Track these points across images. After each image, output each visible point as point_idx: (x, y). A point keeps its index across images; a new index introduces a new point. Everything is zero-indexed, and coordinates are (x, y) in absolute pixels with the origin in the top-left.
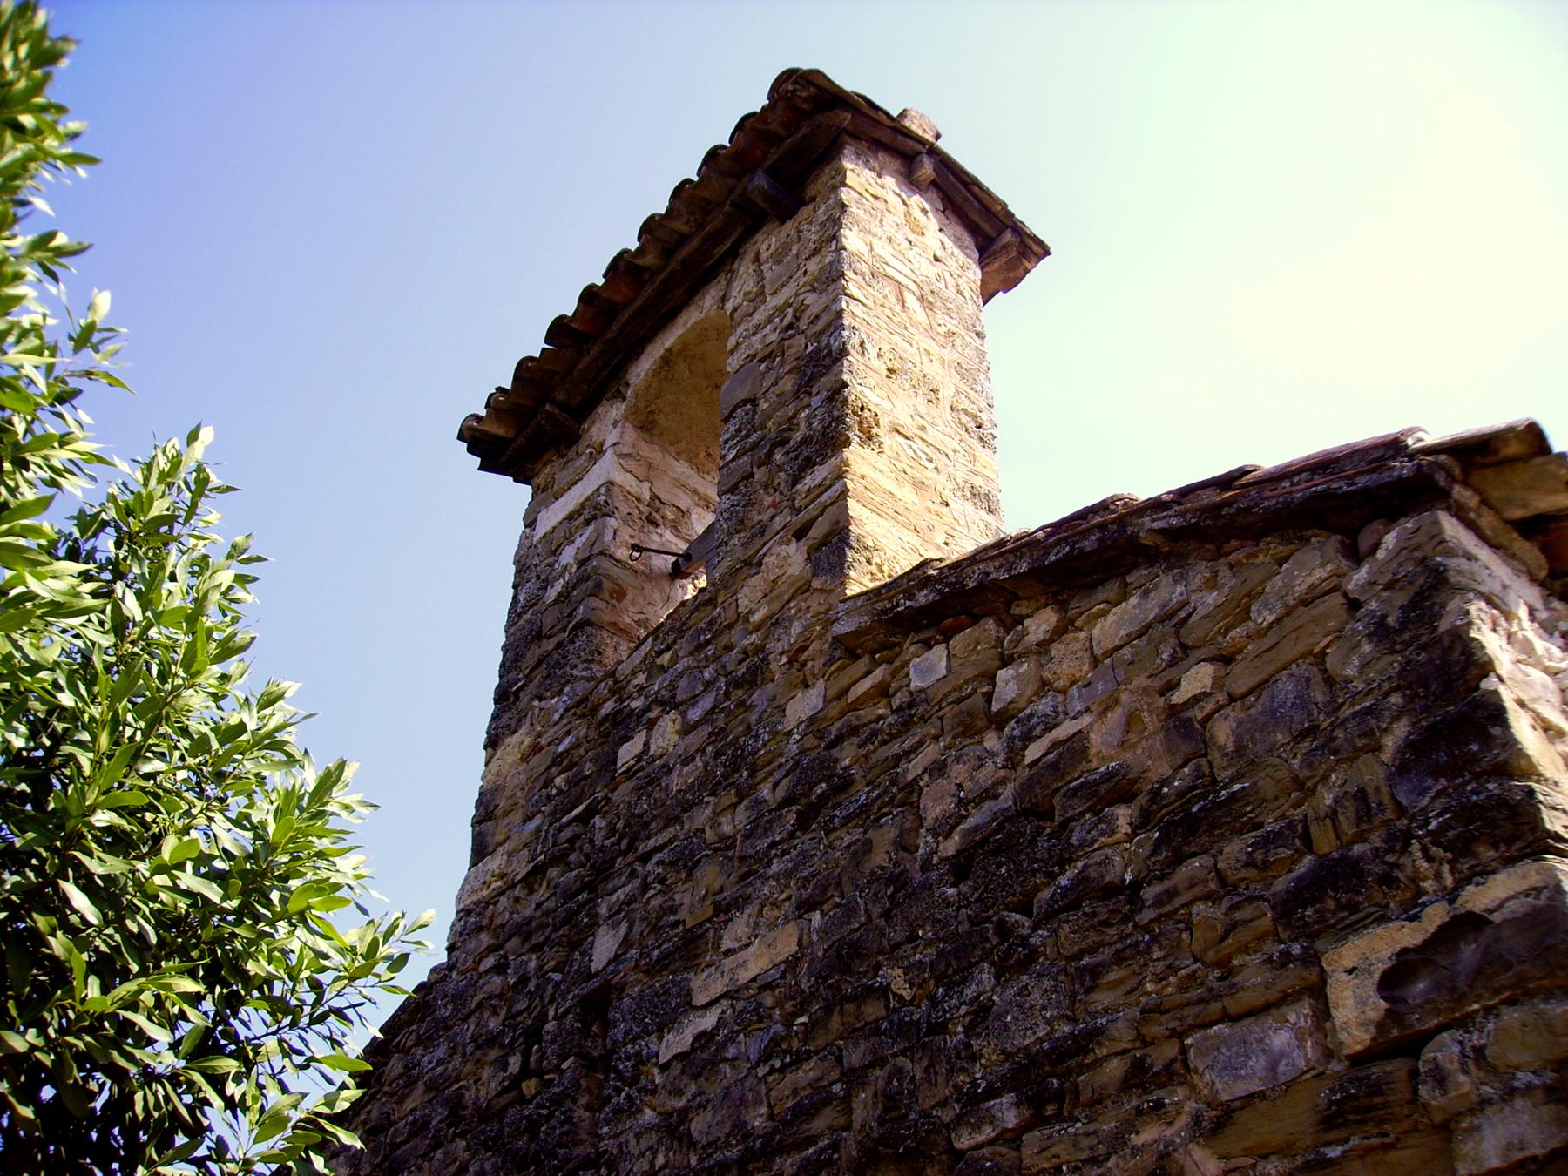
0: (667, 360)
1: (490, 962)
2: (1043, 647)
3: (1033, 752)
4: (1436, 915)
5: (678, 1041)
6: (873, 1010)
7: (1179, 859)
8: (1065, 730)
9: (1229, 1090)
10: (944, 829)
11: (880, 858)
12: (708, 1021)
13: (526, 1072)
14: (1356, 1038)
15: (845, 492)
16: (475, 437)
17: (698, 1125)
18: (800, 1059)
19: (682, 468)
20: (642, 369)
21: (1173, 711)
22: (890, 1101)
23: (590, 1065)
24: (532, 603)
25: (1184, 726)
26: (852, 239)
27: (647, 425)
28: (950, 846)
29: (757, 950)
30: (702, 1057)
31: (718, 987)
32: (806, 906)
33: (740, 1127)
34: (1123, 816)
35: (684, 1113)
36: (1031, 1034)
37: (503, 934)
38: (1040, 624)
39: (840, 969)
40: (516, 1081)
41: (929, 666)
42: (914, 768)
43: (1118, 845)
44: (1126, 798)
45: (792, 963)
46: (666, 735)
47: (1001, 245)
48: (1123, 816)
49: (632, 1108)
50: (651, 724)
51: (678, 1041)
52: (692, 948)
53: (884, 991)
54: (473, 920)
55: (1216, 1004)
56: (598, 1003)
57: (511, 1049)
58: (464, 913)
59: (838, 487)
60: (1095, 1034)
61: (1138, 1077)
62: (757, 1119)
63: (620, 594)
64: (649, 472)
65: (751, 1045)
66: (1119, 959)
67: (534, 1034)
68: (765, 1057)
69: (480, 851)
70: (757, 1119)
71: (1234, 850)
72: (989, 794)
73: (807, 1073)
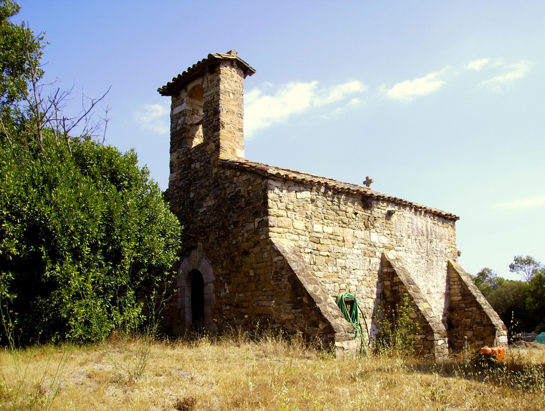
0: (194, 87)
1: (175, 191)
2: (239, 176)
3: (237, 189)
4: (262, 219)
5: (202, 210)
6: (222, 213)
7: (247, 206)
8: (239, 188)
9: (248, 229)
10: (229, 194)
11: (223, 195)
12: (205, 209)
13: (183, 209)
14: (256, 227)
15: (219, 139)
16: (159, 90)
17: (204, 221)
18: (215, 216)
19: (197, 102)
20: (190, 87)
21: (248, 191)
22: (223, 223)
23: (191, 209)
24: (175, 128)
25: (249, 193)
26: (222, 86)
27: (191, 96)
28: (229, 197)
29: (210, 202)
30: (204, 213)
31: (206, 205)
32: (215, 199)
33: (209, 222)
34: (243, 199)
35: (203, 219)
36: (235, 220)
37: (178, 188)
38: (238, 173)
39: (218, 207)
40: (182, 210)
41: (228, 173)
42: (226, 185)
43: (243, 203)
44: (244, 197)
45: (214, 205)
46: (198, 165)
47: (245, 70)
48: (243, 199)
49: (197, 217)
50: (196, 163)
51: (202, 210)
52: (203, 199)
53: (222, 211)
54: (172, 183)
55: (247, 221)
56: (192, 202)
57: (180, 205)
58: (170, 182)
59: (217, 138)
60: (239, 221)
61: (242, 226)
62: (211, 222)
63: (189, 131)
64: (192, 104)
65: (209, 213)
66: (242, 214)
67: (183, 204)
68: (211, 215)
69: (172, 172)
70: (211, 222)
71: (251, 207)
72: (233, 192)
73: (215, 218)
